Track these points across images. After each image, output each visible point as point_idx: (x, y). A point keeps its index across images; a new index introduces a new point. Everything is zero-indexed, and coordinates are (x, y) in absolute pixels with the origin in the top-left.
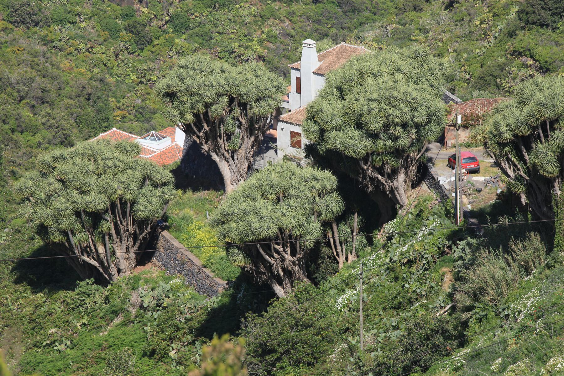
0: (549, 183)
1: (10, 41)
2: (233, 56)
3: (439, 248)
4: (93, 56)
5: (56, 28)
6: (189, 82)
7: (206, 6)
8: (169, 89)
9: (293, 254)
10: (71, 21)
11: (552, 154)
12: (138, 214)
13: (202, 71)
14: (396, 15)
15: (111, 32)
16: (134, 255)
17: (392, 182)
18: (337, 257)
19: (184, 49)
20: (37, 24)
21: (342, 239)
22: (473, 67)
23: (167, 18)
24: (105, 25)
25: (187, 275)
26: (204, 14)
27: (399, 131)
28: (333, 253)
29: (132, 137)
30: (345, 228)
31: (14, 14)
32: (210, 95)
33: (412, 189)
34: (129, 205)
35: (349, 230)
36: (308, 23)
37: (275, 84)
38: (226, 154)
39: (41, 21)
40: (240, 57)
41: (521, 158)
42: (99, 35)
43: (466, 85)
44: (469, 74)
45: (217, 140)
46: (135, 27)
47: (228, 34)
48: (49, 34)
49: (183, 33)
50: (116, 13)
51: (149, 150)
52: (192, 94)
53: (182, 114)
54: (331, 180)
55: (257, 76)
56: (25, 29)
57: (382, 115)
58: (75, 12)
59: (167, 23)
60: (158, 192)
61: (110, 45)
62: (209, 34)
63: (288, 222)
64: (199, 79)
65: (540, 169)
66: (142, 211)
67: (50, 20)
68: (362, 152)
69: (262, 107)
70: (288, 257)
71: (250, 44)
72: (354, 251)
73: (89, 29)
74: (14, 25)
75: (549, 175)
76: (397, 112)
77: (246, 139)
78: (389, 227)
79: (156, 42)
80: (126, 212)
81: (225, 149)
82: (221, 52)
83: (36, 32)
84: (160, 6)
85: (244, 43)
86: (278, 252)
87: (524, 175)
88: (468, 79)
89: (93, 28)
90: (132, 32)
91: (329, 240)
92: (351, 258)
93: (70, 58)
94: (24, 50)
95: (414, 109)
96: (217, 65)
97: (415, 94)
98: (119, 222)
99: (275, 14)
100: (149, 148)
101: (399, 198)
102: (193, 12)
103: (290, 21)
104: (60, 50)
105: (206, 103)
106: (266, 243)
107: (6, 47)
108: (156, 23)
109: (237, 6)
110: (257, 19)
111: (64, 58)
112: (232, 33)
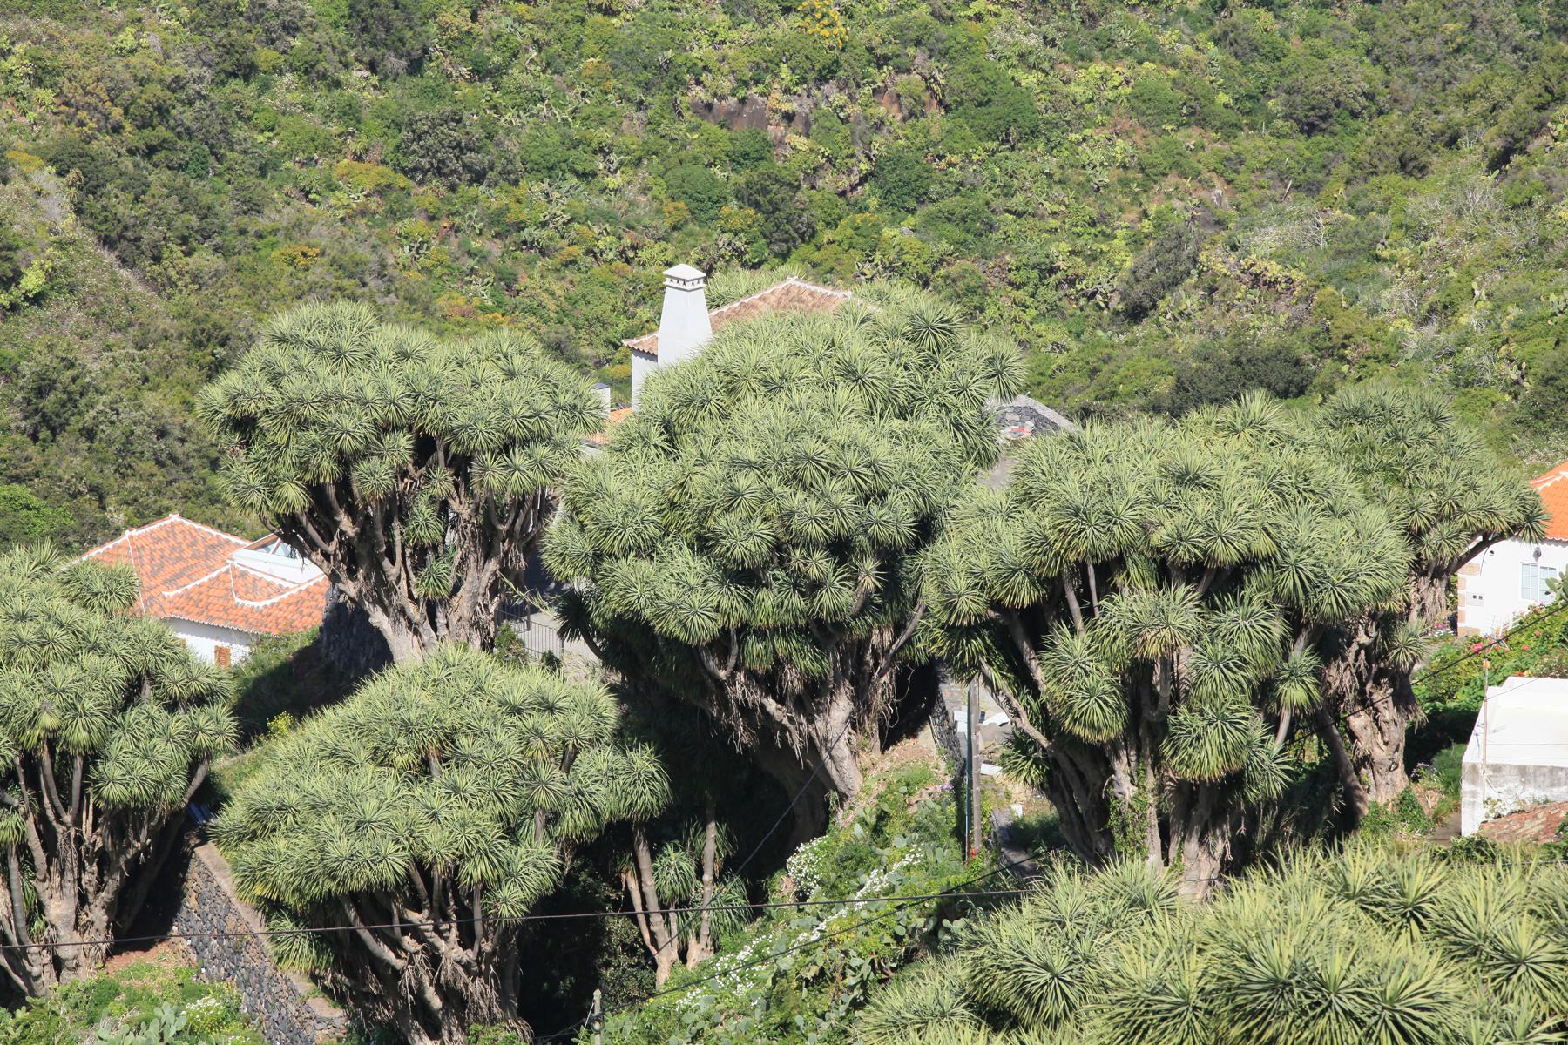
0: (1101, 757)
1: (286, 228)
2: (1052, 280)
3: (898, 939)
4: (637, 270)
5: (536, 189)
6: (294, 385)
7: (983, 133)
8: (235, 407)
9: (467, 940)
10: (579, 168)
11: (1103, 667)
12: (105, 791)
13: (339, 354)
14: (1348, 182)
15: (694, 205)
16: (105, 918)
17: (811, 721)
18: (652, 949)
19: (906, 258)
20: (478, 177)
21: (668, 893)
22: (1530, 347)
23: (865, 166)
24: (679, 182)
25: (246, 983)
26: (975, 157)
27: (819, 564)
28: (640, 934)
29: (228, 542)
30: (674, 858)
31: (415, 146)
32: (353, 426)
33: (884, 747)
34: (78, 763)
35: (688, 867)
36: (1280, 191)
37: (565, 399)
38: (411, 609)
39: (492, 169)
40: (1072, 284)
41: (1024, 680)
42: (658, 211)
43: (1508, 398)
44: (1520, 368)
45: (380, 568)
46: (764, 191)
47: (1042, 217)
48: (513, 206)
49: (908, 211)
50: (715, 150)
51: (269, 584)
52: (303, 424)
53: (272, 485)
54: (593, 710)
55: (511, 374)
56: (443, 189)
57: (769, 511)
58: (594, 145)
59: (863, 180)
60: (177, 723)
61: (691, 241)
62: (983, 216)
63: (438, 842)
64: (329, 378)
65: (1066, 716)
66: (121, 779)
67: (519, 165)
68: (704, 626)
69: (516, 468)
70: (451, 951)
71: (1105, 248)
72: (704, 932)
73: (630, 193)
74: (412, 178)
75: (1089, 735)
76: (813, 506)
77: (473, 565)
78: (805, 860)
79: (826, 235)
80: (70, 783)
81: (410, 596)
82: (1018, 269)
83: (475, 200)
84: (845, 130)
85: (1088, 243)
86: (418, 935)
87: (1035, 733)
88: (1517, 382)
89: (644, 191)
90: (757, 206)
91: (628, 893)
92: (696, 953)
93: (570, 277)
94: (323, 254)
95: (871, 496)
96: (387, 337)
97: (882, 451)
98: (50, 813)
99: (1183, 161)
100: (269, 579)
101: (833, 773)
102: (940, 149)
103: (1229, 182)
104: (543, 253)
105: (341, 452)
106: (375, 903)
107: (273, 246)
108: (829, 181)
109: (1073, 137)
110: (1131, 174)
111: (551, 277)
112: (1054, 214)
